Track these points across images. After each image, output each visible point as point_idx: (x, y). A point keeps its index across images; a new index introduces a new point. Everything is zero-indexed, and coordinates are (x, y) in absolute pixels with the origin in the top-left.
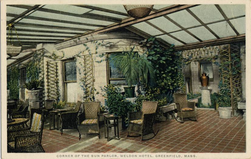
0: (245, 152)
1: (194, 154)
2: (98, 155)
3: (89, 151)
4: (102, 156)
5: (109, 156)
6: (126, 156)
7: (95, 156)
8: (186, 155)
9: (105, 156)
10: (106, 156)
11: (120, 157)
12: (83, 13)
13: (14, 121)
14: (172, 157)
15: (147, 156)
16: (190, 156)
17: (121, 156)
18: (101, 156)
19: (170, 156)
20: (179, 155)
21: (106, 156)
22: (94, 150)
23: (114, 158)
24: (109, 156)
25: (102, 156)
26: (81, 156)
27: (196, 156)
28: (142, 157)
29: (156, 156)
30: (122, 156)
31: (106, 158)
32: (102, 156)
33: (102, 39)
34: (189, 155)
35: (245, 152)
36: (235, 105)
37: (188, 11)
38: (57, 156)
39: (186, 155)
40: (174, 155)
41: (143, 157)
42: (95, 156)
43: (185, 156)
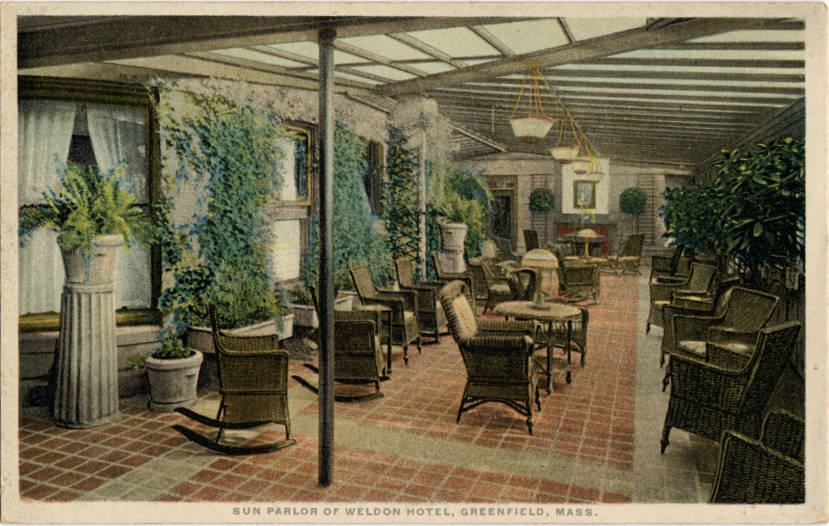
0: (803, 502)
1: (359, 507)
2: (255, 509)
3: (339, 496)
4: (270, 510)
5: (292, 512)
6: (364, 512)
7: (247, 511)
8: (563, 510)
9: (572, 514)
10: (282, 510)
11: (459, 516)
12: (154, 67)
13: (548, 309)
14: (516, 513)
15: (433, 512)
16: (574, 512)
17: (348, 514)
18: (266, 511)
19: (509, 511)
20: (375, 510)
21: (282, 510)
22: (153, 495)
23: (584, 518)
24: (292, 512)
25: (270, 510)
26: (403, 513)
27: (594, 512)
28: (392, 510)
29: (464, 513)
30: (352, 513)
31: (282, 517)
32: (269, 512)
33: (279, 85)
34: (279, 509)
35: (803, 502)
36: (752, 281)
37: (307, 19)
38: (236, 511)
39: (563, 510)
40: (522, 510)
41: (387, 515)
42: (247, 511)
43: (558, 510)
